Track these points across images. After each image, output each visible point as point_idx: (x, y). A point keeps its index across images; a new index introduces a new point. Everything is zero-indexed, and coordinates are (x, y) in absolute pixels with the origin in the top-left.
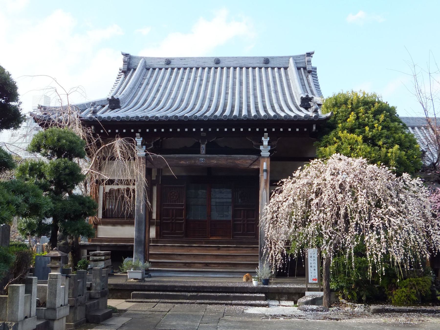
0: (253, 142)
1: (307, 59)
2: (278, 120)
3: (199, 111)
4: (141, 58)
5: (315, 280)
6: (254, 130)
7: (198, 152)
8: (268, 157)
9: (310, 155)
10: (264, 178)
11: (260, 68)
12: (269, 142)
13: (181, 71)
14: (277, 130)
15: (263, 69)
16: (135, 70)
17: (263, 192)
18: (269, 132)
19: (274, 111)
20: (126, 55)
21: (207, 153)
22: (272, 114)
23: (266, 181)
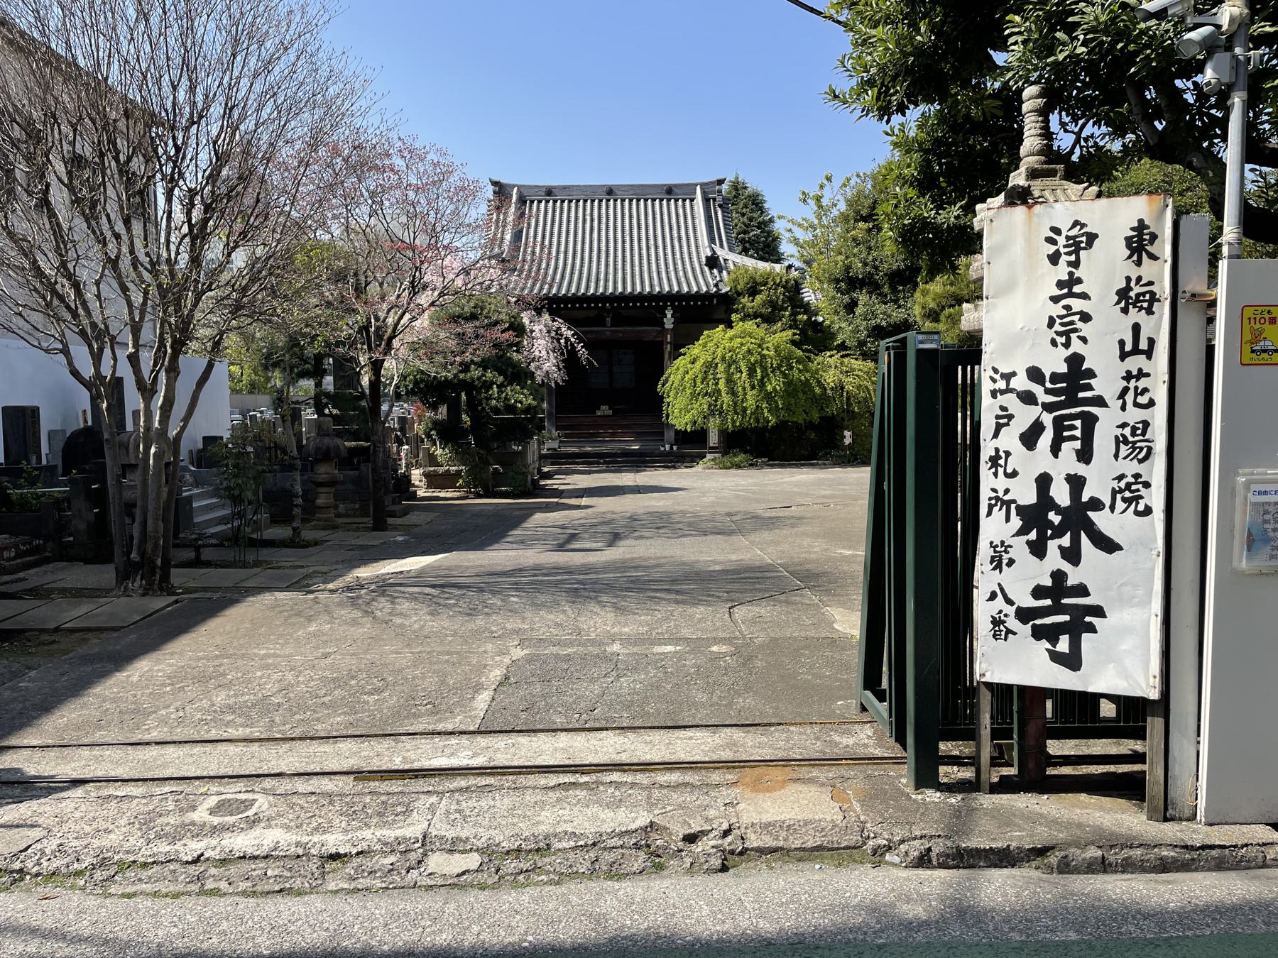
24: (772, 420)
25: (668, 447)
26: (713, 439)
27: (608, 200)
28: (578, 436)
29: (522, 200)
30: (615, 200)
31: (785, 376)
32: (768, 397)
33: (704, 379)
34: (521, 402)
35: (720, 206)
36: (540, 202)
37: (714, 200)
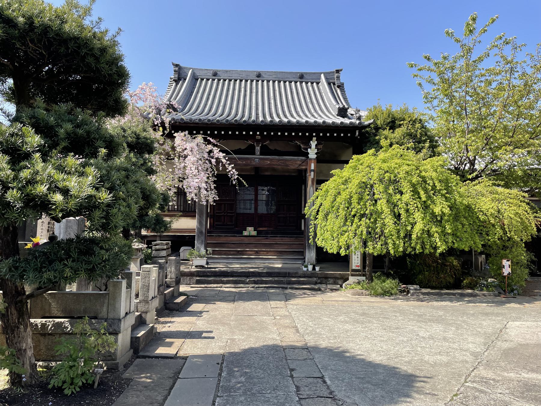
0: (302, 145)
1: (336, 75)
2: (326, 126)
3: (221, 115)
4: (190, 69)
5: (358, 266)
6: (304, 134)
7: (254, 153)
8: (314, 159)
9: (343, 158)
10: (311, 176)
11: (296, 82)
12: (316, 145)
13: (232, 83)
14: (325, 135)
15: (298, 83)
16: (185, 79)
17: (310, 188)
18: (318, 136)
19: (278, 115)
20: (177, 65)
21: (261, 154)
22: (277, 120)
23: (313, 180)
24: (442, 248)
25: (310, 268)
26: (356, 262)
27: (258, 81)
28: (226, 253)
29: (195, 78)
30: (263, 81)
31: (447, 199)
32: (438, 220)
33: (360, 199)
34: (65, 192)
35: (338, 87)
36: (208, 80)
37: (334, 84)
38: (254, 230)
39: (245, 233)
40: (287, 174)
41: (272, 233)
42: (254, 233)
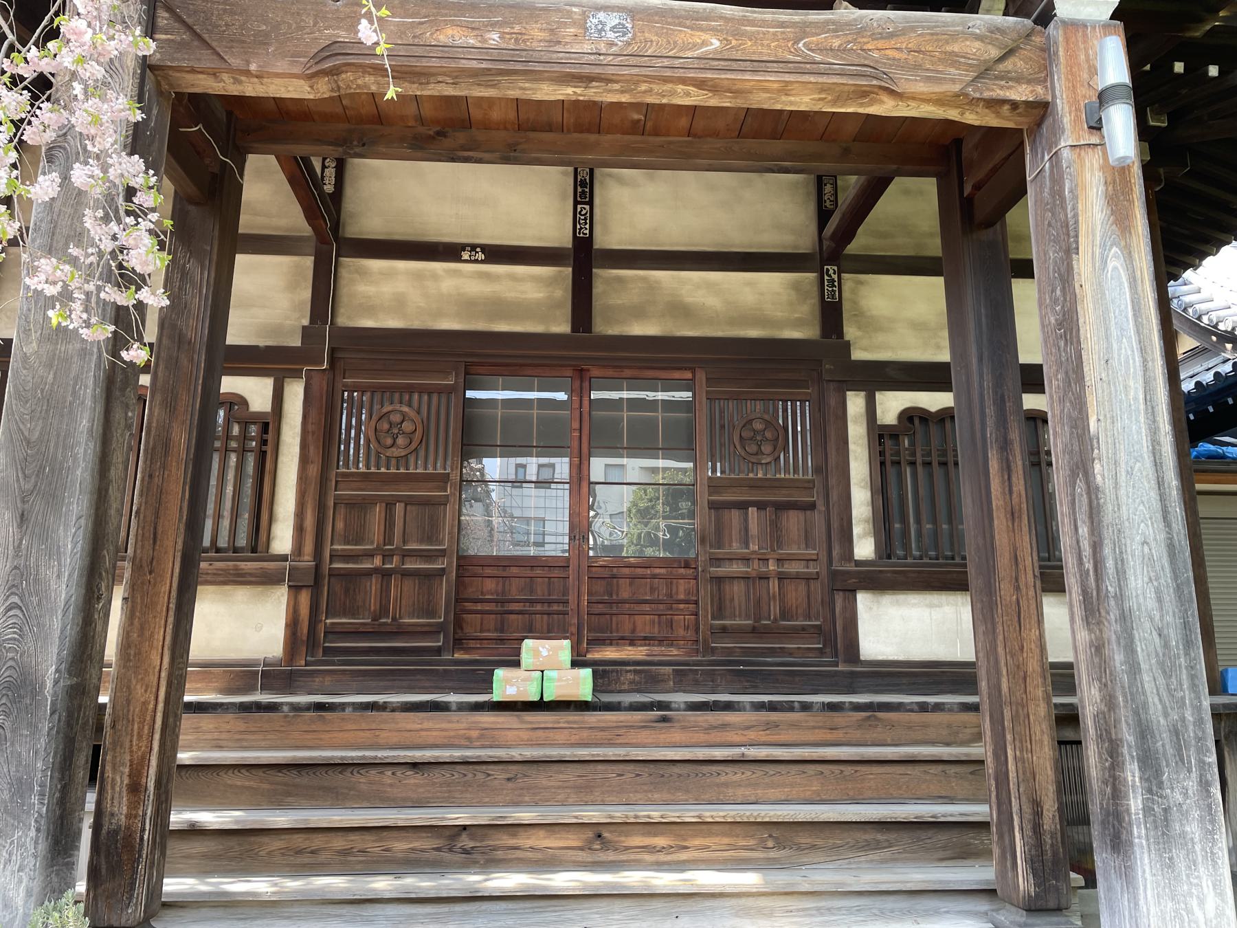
38: (575, 664)
39: (507, 684)
40: (754, 333)
41: (684, 677)
42: (582, 684)
